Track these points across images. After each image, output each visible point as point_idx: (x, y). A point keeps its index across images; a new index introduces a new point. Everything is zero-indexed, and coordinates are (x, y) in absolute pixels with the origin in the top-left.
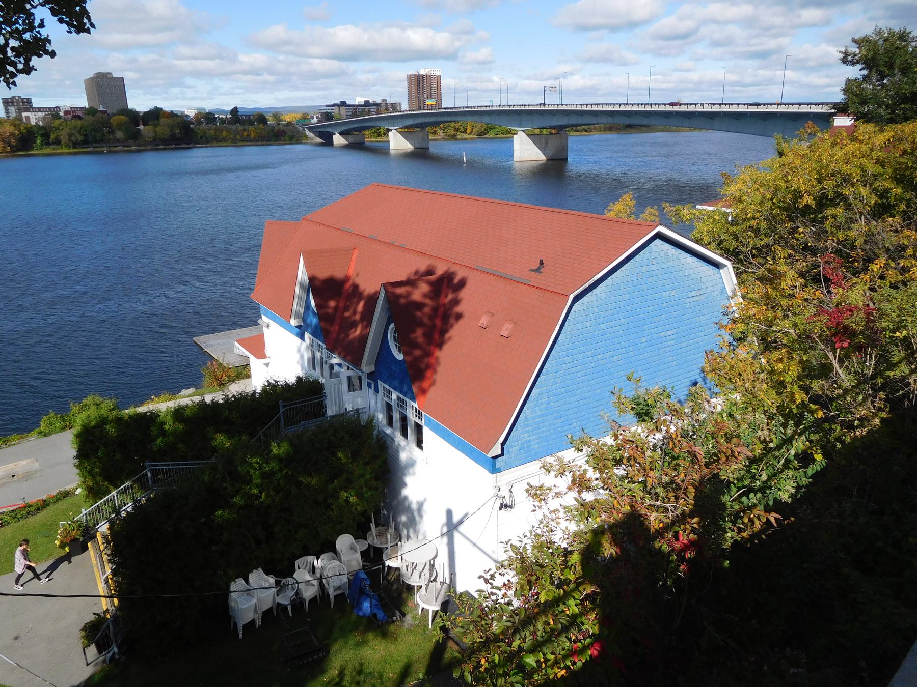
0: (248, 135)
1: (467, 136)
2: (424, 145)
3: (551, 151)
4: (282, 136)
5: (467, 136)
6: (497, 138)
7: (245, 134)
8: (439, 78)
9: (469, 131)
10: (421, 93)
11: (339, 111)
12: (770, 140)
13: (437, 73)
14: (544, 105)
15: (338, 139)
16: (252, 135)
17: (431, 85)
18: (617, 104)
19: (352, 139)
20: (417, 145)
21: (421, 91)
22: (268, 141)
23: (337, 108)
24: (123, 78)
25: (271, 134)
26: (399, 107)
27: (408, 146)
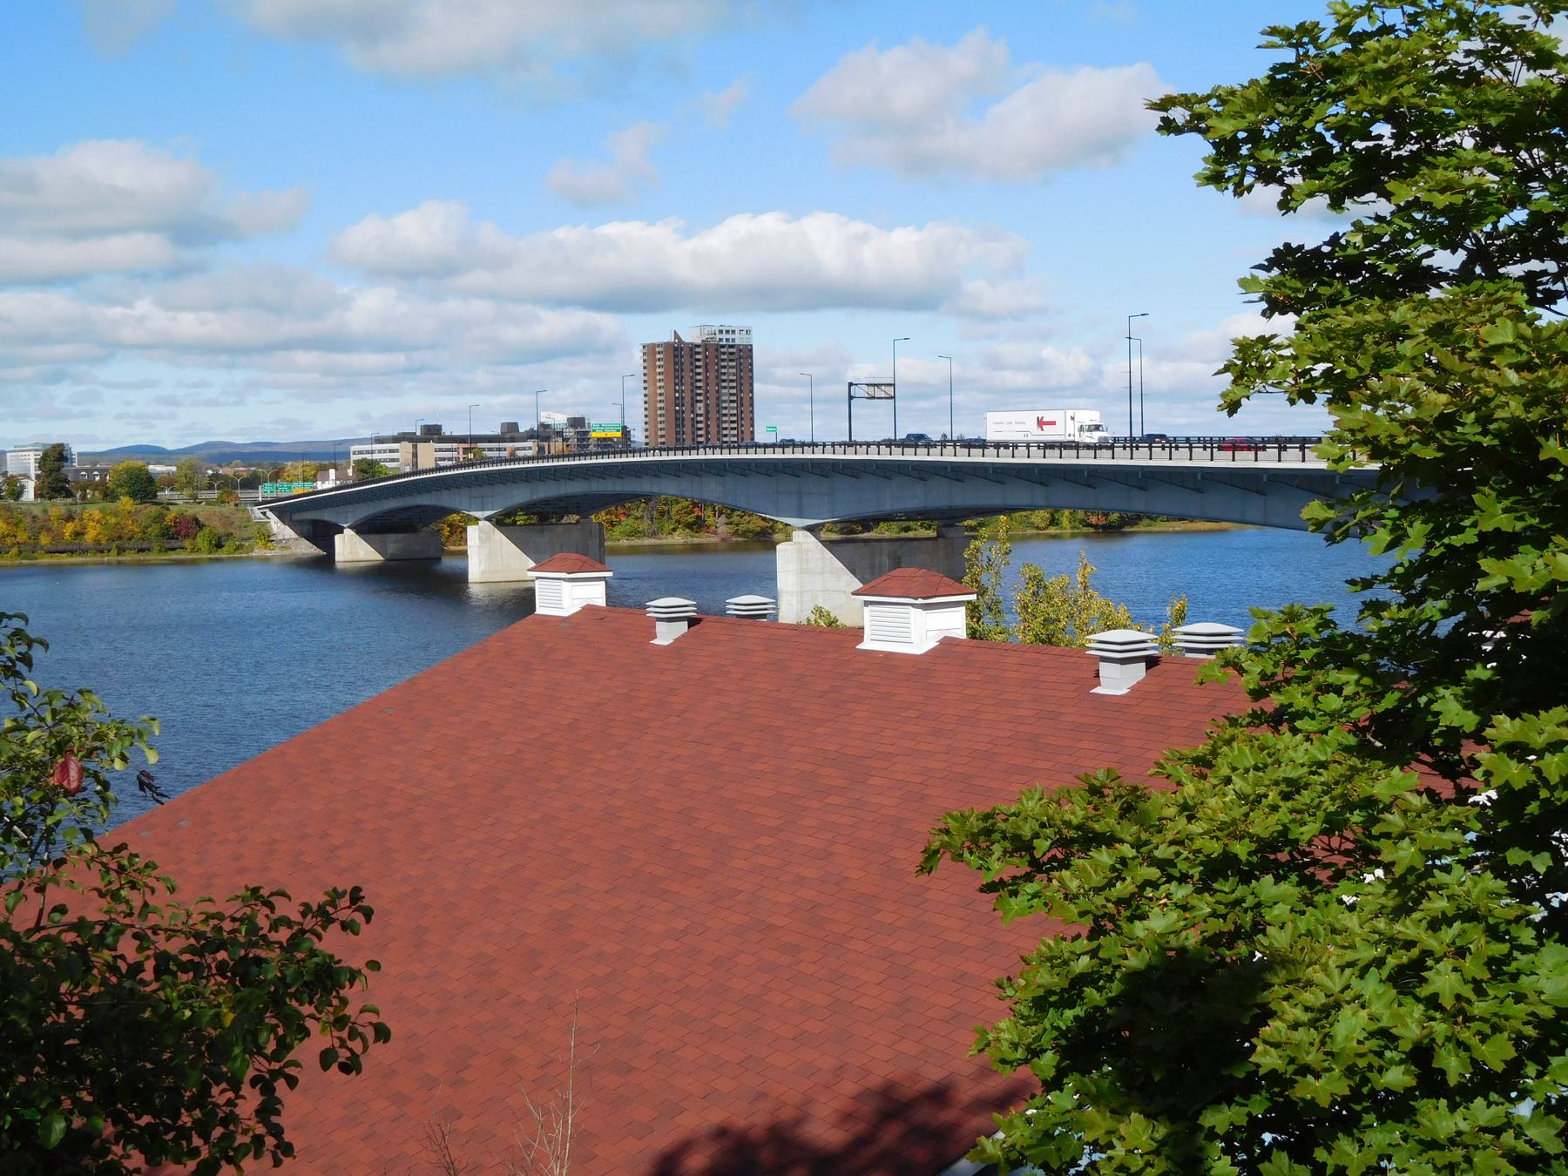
0: (78, 534)
4: (187, 536)
7: (69, 529)
10: (687, 400)
11: (415, 455)
14: (851, 444)
15: (351, 549)
16: (91, 535)
17: (719, 374)
18: (1291, 440)
19: (395, 543)
21: (687, 395)
22: (141, 550)
23: (406, 447)
24: (747, 351)
25: (154, 530)
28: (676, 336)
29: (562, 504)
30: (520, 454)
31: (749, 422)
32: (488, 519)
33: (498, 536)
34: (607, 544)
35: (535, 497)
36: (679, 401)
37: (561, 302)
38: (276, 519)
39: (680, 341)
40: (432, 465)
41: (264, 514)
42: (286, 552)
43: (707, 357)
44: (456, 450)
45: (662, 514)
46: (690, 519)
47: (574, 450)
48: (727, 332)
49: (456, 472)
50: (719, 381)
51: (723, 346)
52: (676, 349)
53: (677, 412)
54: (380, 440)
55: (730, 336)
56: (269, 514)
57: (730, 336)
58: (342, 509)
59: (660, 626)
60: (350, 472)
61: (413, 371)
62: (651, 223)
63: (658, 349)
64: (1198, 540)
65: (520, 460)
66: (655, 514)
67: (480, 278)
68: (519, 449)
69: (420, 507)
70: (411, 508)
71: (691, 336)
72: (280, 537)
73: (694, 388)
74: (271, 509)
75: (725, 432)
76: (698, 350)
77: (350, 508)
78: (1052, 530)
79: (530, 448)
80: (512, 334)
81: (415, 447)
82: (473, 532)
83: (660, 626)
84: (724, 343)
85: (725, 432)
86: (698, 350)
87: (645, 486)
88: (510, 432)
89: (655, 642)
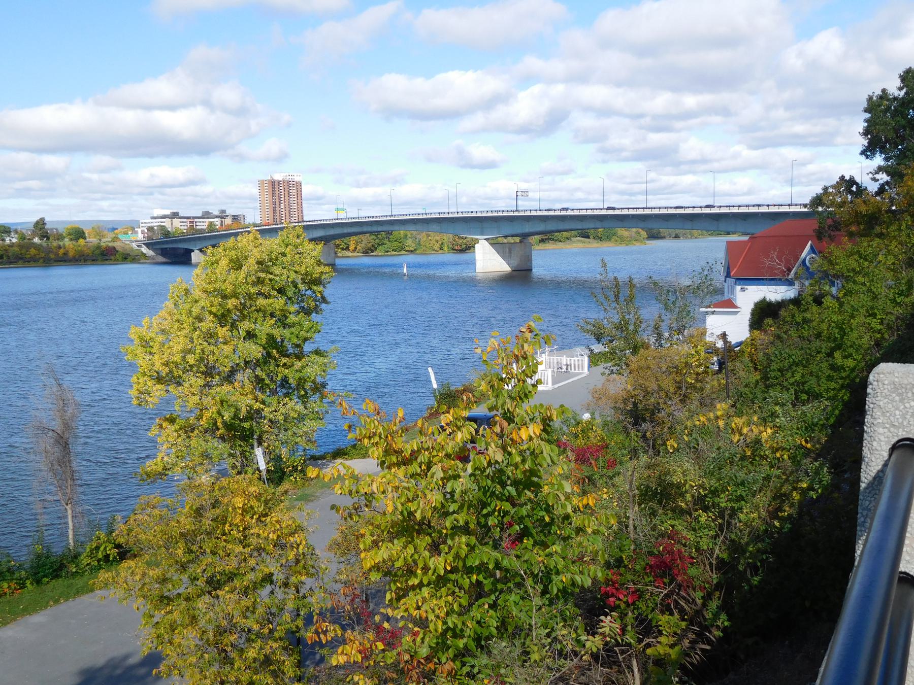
1: (350, 254)
3: (515, 262)
4: (111, 254)
5: (350, 254)
6: (388, 255)
8: (299, 185)
9: (352, 247)
10: (277, 203)
11: (172, 224)
12: (311, 454)
13: (297, 179)
16: (887, 187)
21: (277, 201)
26: (242, 220)
36: (274, 203)
50: (289, 195)
64: (5, 270)
73: (279, 198)
78: (441, 252)
88: (222, 215)
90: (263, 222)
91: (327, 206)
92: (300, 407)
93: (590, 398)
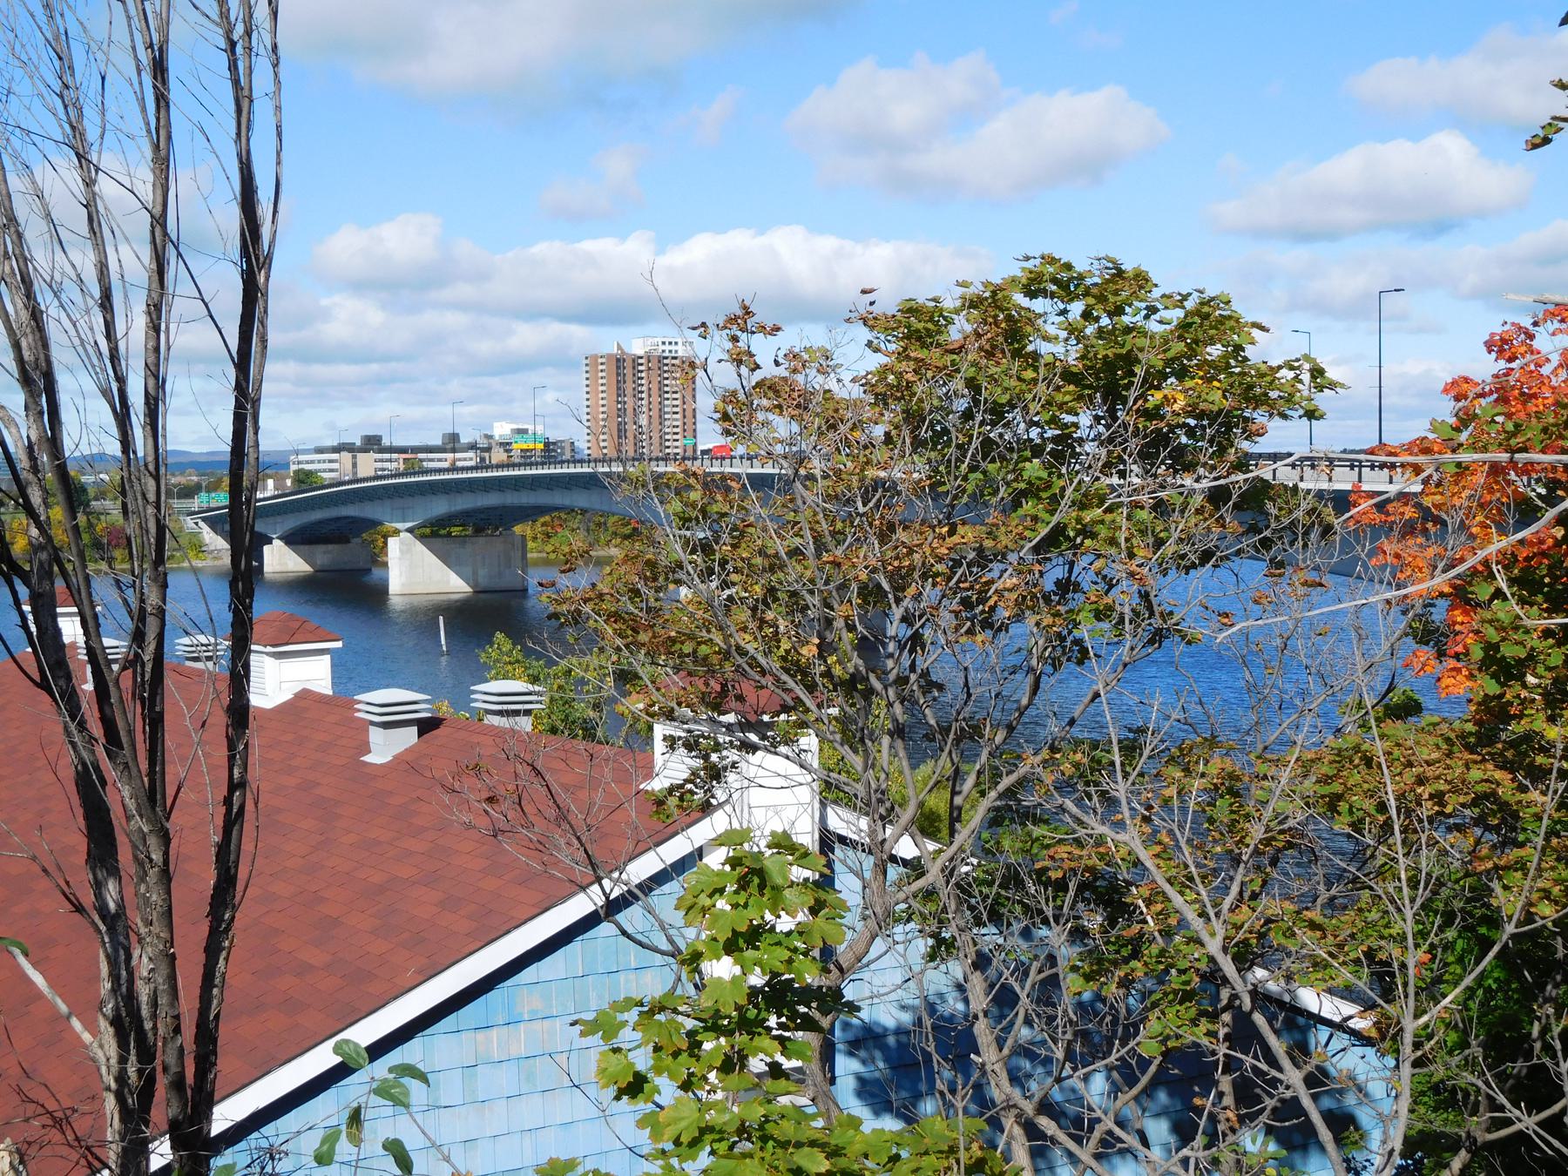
2: (507, 582)
10: (630, 411)
11: (354, 465)
17: (661, 385)
19: (326, 555)
20: (484, 582)
23: (346, 457)
27: (453, 584)
28: (619, 347)
29: (482, 516)
30: (459, 464)
31: (691, 433)
32: (410, 530)
33: (420, 548)
34: (529, 555)
35: (453, 509)
36: (621, 412)
37: (533, 313)
38: (208, 529)
39: (623, 352)
40: (372, 474)
41: (196, 524)
42: (217, 563)
43: (649, 369)
44: (396, 460)
45: (599, 525)
46: (628, 530)
47: (517, 460)
48: (670, 343)
49: (376, 483)
50: (662, 392)
51: (666, 358)
52: (618, 360)
53: (620, 423)
54: (320, 451)
55: (673, 348)
56: (201, 524)
57: (673, 348)
58: (271, 520)
59: (376, 735)
60: (289, 482)
61: (382, 382)
62: (623, 237)
63: (600, 360)
65: (463, 469)
66: (592, 526)
67: (465, 291)
68: (460, 460)
69: (346, 518)
70: (338, 519)
71: (637, 348)
72: (212, 548)
74: (204, 519)
75: (667, 444)
76: (640, 361)
77: (279, 519)
79: (471, 459)
80: (485, 347)
81: (354, 457)
82: (393, 543)
83: (376, 735)
84: (667, 354)
85: (667, 444)
86: (640, 361)
87: (558, 498)
88: (452, 442)
89: (368, 758)
90: (595, 454)
91: (473, 409)
92: (860, 768)
93: (1489, 380)
